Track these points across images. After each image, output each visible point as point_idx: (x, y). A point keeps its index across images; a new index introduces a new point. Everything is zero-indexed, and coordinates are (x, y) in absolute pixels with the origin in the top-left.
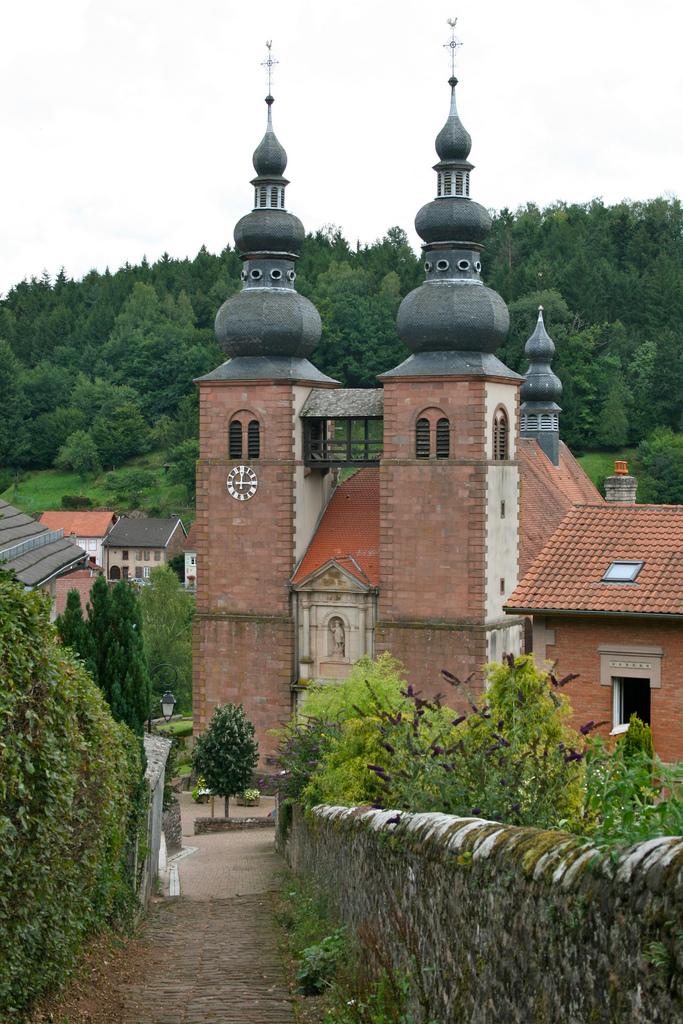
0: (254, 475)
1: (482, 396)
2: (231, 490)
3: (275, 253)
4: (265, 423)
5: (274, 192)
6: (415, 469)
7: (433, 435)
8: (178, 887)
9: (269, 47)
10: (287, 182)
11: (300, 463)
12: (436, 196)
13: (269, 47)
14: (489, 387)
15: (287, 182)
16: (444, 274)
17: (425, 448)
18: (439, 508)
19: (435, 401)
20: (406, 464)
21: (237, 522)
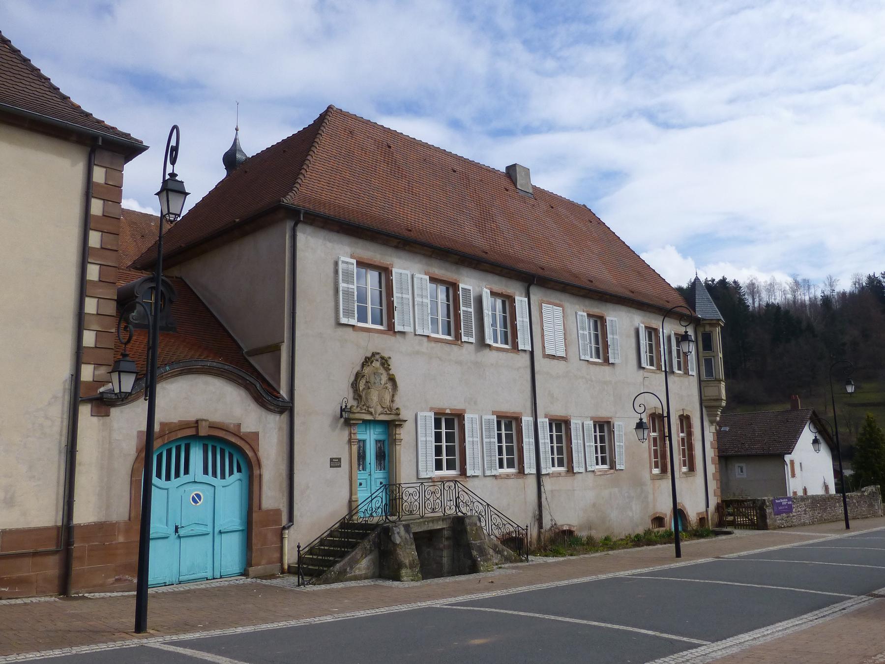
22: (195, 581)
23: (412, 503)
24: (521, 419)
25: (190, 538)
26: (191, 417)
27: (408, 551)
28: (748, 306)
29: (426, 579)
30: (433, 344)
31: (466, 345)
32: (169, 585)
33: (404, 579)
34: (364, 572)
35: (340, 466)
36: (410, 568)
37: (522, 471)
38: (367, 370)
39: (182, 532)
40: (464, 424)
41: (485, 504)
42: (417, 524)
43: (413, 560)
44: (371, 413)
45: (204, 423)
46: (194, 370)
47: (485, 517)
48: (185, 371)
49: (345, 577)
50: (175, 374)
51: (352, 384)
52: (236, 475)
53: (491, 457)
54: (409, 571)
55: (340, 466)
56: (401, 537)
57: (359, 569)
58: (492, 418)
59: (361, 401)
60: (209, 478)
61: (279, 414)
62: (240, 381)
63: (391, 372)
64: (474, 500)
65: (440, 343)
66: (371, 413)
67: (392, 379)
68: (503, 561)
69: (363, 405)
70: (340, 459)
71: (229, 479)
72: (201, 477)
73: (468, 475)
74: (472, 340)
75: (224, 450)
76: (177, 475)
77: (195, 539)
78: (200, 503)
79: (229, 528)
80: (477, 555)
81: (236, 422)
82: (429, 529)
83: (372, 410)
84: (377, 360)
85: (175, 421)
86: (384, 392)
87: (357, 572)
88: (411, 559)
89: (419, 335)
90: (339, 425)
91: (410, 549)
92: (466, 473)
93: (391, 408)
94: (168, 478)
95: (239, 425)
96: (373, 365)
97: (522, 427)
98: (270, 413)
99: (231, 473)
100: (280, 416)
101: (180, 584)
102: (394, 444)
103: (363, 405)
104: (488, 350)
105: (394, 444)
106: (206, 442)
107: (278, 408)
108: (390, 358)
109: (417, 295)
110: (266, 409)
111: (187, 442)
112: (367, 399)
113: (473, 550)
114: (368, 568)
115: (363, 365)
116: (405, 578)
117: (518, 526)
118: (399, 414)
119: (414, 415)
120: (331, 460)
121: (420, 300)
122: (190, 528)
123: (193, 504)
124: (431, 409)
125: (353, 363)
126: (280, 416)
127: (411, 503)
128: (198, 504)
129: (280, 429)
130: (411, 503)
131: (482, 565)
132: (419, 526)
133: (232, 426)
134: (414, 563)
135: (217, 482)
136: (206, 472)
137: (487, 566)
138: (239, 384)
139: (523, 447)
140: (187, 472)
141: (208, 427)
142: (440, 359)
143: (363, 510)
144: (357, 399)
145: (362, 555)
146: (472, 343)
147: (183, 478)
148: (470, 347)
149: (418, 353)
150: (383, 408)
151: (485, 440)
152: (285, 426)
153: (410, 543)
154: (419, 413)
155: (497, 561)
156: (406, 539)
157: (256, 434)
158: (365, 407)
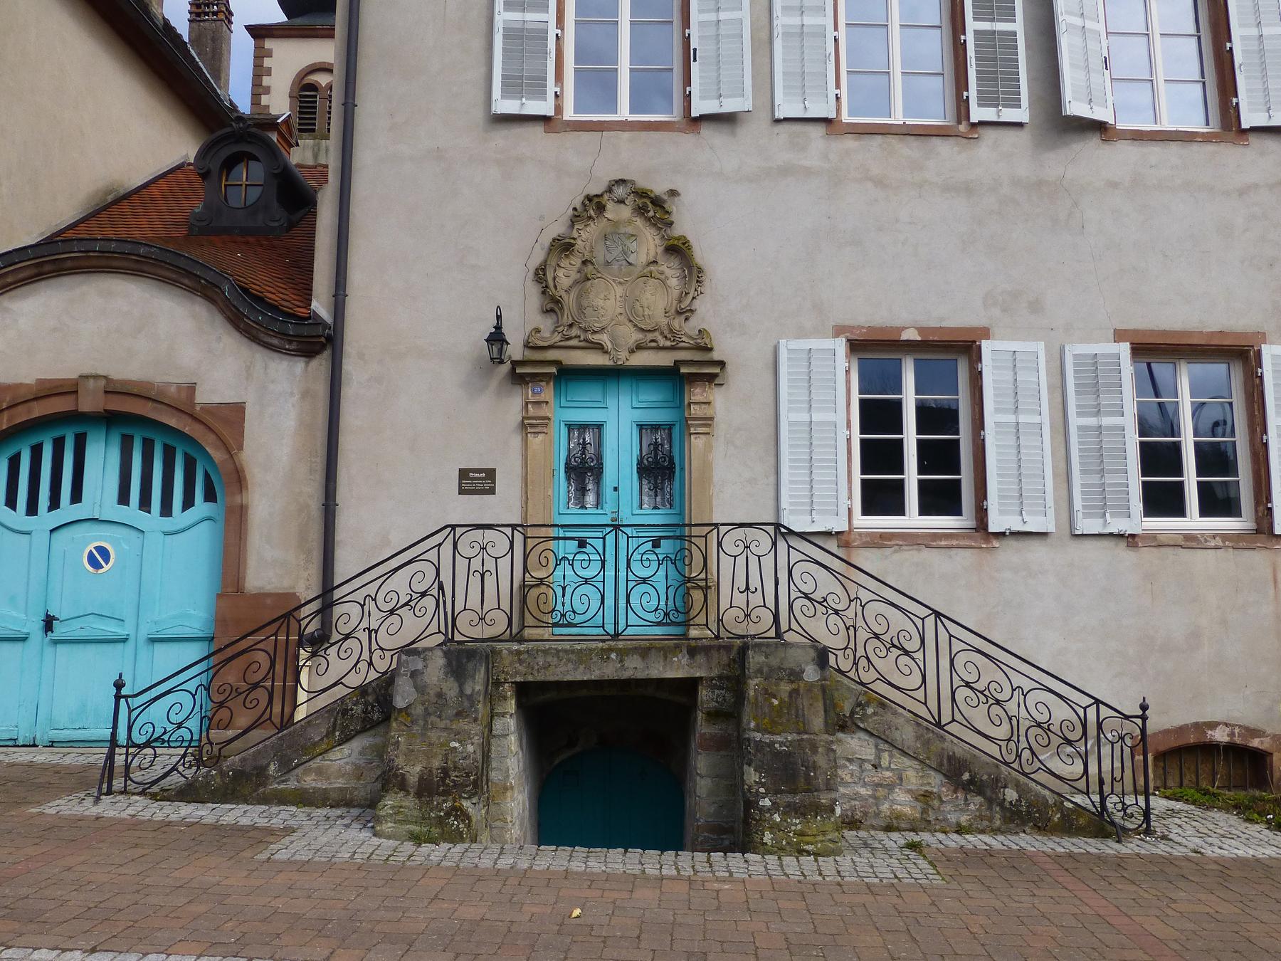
22: (87, 745)
23: (569, 591)
24: (1259, 354)
25: (81, 646)
26: (65, 370)
27: (433, 736)
29: (559, 842)
30: (850, 143)
31: (990, 135)
32: (24, 746)
33: (384, 826)
34: (339, 783)
35: (492, 491)
36: (419, 795)
37: (1265, 526)
38: (587, 235)
39: (59, 630)
40: (981, 373)
41: (924, 612)
42: (573, 657)
43: (445, 772)
44: (599, 347)
45: (91, 382)
46: (69, 264)
47: (919, 656)
48: (47, 268)
49: (261, 790)
50: (21, 275)
51: (536, 274)
52: (201, 506)
53: (1103, 476)
54: (410, 802)
55: (492, 491)
56: (421, 689)
57: (320, 772)
58: (1116, 351)
59: (562, 316)
60: (132, 512)
61: (303, 359)
62: (186, 281)
63: (677, 231)
64: (865, 596)
65: (880, 136)
66: (599, 347)
67: (678, 250)
68: (998, 823)
69: (571, 326)
70: (491, 474)
71: (180, 517)
72: (112, 510)
73: (991, 530)
74: (1021, 114)
75: (174, 449)
76: (54, 504)
77: (92, 648)
78: (106, 568)
79: (169, 631)
80: (763, 785)
81: (183, 379)
82: (626, 675)
83: (604, 338)
84: (621, 202)
85: (27, 381)
86: (642, 284)
87: (311, 782)
88: (437, 763)
89: (786, 120)
90: (494, 383)
91: (446, 729)
92: (987, 526)
93: (671, 331)
94: (32, 509)
95: (192, 388)
96: (608, 215)
97: (1261, 378)
98: (275, 355)
99: (188, 503)
100: (307, 364)
101: (52, 746)
102: (686, 433)
103: (571, 326)
104: (1099, 141)
105: (686, 433)
106: (128, 431)
107: (290, 342)
108: (673, 193)
109: (784, 8)
110: (259, 344)
111: (80, 430)
112: (581, 308)
113: (749, 765)
114: (358, 773)
115: (577, 217)
116: (387, 827)
117: (1098, 702)
118: (711, 349)
119: (771, 349)
120: (464, 474)
121: (795, 20)
122: (76, 624)
123: (91, 569)
124: (838, 331)
125: (542, 218)
126: (307, 364)
127: (564, 588)
128: (101, 571)
129: (306, 394)
130: (564, 588)
131: (774, 828)
132: (580, 662)
133: (173, 389)
134: (443, 779)
135: (152, 521)
136: (124, 498)
137: (802, 834)
138: (192, 290)
139: (1266, 445)
140: (76, 497)
141: (101, 394)
142: (880, 182)
143: (359, 596)
144: (552, 310)
145: (330, 733)
146: (1019, 125)
147: (67, 511)
148: (1021, 137)
149: (786, 171)
150: (642, 330)
151: (1075, 421)
152: (322, 389)
153: (451, 712)
154: (783, 342)
155: (964, 819)
156: (440, 695)
157: (239, 409)
158: (574, 332)
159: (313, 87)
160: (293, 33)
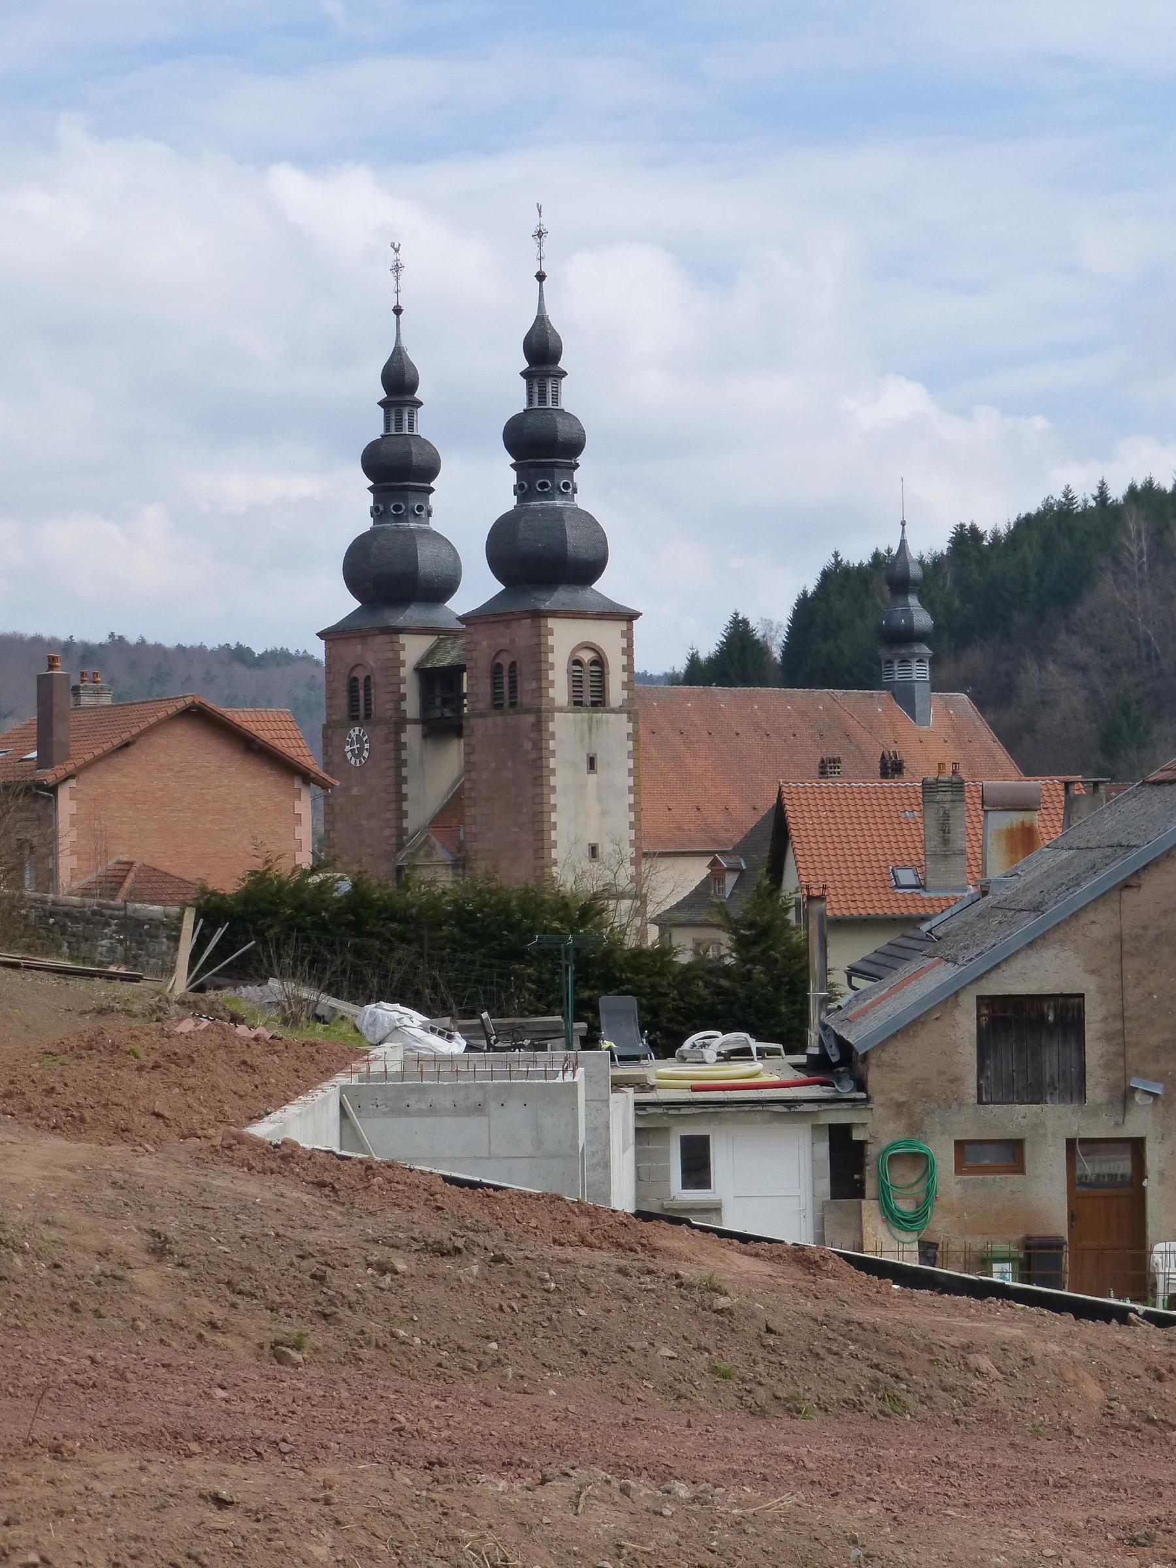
0: (366, 737)
1: (397, 649)
2: (349, 755)
3: (394, 484)
4: (377, 678)
5: (411, 414)
6: (490, 720)
7: (506, 681)
8: (999, 1249)
9: (397, 251)
10: (565, 374)
11: (415, 722)
12: (525, 407)
13: (397, 251)
14: (403, 639)
15: (565, 374)
16: (398, 518)
17: (576, 684)
18: (509, 764)
19: (504, 642)
20: (483, 715)
21: (355, 791)
28: (403, 664)
159: (577, 662)
160: (570, 615)
